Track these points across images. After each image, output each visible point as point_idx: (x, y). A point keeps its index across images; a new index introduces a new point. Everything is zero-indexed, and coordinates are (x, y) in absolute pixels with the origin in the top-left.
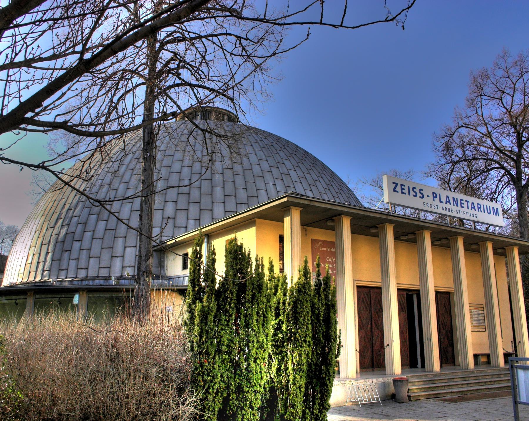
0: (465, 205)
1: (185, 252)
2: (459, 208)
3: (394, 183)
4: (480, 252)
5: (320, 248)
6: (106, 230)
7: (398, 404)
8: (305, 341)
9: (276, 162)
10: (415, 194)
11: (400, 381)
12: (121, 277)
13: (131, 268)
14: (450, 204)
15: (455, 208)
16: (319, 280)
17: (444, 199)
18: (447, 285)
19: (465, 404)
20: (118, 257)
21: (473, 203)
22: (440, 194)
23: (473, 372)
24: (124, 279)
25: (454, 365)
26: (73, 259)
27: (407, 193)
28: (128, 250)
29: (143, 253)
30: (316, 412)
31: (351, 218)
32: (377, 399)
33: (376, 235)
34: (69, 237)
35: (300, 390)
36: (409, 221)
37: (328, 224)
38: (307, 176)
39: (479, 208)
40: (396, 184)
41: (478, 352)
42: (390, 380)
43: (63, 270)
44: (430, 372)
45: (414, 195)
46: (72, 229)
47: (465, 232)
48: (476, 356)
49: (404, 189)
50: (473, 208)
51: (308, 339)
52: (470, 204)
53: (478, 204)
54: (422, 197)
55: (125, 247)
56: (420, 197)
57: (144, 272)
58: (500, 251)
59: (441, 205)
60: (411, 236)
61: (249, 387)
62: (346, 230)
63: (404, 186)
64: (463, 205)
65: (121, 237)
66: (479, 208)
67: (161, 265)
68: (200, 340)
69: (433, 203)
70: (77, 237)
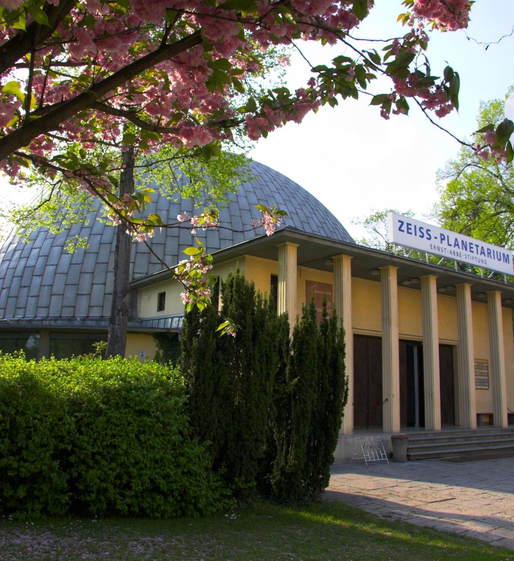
0: (474, 249)
1: (162, 291)
2: (468, 253)
3: (399, 221)
4: (487, 302)
5: (315, 290)
6: (70, 264)
7: (396, 464)
8: (311, 386)
9: (265, 195)
10: (421, 235)
11: (401, 438)
12: (87, 318)
13: (98, 308)
14: (459, 248)
15: (463, 252)
16: (326, 320)
17: (452, 242)
18: (451, 338)
19: (468, 465)
20: (84, 295)
21: (482, 248)
22: (448, 236)
23: (475, 432)
24: (91, 320)
25: (454, 425)
26: (32, 297)
27: (413, 233)
28: (95, 287)
29: (119, 289)
30: (320, 465)
31: (352, 257)
32: (384, 456)
33: (377, 279)
34: (28, 271)
35: (304, 440)
36: (414, 264)
37: (326, 264)
38: (299, 211)
39: (489, 253)
40: (402, 223)
41: (479, 412)
42: (389, 438)
43: (20, 308)
44: (430, 430)
45: (420, 236)
46: (31, 262)
47: (474, 279)
48: (478, 415)
49: (410, 229)
50: (483, 253)
51: (314, 384)
52: (479, 249)
53: (488, 249)
54: (429, 239)
55: (93, 284)
56: (427, 238)
57: (120, 310)
58: (508, 302)
59: (449, 248)
60: (414, 281)
61: (250, 435)
62: (346, 273)
63: (410, 225)
64: (472, 250)
65: (88, 273)
66: (489, 253)
67: (134, 305)
68: (196, 382)
69: (441, 246)
70: (37, 272)
